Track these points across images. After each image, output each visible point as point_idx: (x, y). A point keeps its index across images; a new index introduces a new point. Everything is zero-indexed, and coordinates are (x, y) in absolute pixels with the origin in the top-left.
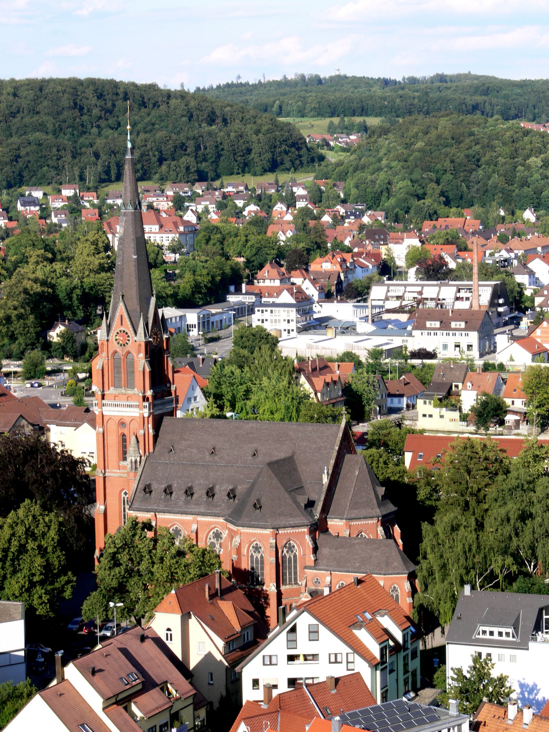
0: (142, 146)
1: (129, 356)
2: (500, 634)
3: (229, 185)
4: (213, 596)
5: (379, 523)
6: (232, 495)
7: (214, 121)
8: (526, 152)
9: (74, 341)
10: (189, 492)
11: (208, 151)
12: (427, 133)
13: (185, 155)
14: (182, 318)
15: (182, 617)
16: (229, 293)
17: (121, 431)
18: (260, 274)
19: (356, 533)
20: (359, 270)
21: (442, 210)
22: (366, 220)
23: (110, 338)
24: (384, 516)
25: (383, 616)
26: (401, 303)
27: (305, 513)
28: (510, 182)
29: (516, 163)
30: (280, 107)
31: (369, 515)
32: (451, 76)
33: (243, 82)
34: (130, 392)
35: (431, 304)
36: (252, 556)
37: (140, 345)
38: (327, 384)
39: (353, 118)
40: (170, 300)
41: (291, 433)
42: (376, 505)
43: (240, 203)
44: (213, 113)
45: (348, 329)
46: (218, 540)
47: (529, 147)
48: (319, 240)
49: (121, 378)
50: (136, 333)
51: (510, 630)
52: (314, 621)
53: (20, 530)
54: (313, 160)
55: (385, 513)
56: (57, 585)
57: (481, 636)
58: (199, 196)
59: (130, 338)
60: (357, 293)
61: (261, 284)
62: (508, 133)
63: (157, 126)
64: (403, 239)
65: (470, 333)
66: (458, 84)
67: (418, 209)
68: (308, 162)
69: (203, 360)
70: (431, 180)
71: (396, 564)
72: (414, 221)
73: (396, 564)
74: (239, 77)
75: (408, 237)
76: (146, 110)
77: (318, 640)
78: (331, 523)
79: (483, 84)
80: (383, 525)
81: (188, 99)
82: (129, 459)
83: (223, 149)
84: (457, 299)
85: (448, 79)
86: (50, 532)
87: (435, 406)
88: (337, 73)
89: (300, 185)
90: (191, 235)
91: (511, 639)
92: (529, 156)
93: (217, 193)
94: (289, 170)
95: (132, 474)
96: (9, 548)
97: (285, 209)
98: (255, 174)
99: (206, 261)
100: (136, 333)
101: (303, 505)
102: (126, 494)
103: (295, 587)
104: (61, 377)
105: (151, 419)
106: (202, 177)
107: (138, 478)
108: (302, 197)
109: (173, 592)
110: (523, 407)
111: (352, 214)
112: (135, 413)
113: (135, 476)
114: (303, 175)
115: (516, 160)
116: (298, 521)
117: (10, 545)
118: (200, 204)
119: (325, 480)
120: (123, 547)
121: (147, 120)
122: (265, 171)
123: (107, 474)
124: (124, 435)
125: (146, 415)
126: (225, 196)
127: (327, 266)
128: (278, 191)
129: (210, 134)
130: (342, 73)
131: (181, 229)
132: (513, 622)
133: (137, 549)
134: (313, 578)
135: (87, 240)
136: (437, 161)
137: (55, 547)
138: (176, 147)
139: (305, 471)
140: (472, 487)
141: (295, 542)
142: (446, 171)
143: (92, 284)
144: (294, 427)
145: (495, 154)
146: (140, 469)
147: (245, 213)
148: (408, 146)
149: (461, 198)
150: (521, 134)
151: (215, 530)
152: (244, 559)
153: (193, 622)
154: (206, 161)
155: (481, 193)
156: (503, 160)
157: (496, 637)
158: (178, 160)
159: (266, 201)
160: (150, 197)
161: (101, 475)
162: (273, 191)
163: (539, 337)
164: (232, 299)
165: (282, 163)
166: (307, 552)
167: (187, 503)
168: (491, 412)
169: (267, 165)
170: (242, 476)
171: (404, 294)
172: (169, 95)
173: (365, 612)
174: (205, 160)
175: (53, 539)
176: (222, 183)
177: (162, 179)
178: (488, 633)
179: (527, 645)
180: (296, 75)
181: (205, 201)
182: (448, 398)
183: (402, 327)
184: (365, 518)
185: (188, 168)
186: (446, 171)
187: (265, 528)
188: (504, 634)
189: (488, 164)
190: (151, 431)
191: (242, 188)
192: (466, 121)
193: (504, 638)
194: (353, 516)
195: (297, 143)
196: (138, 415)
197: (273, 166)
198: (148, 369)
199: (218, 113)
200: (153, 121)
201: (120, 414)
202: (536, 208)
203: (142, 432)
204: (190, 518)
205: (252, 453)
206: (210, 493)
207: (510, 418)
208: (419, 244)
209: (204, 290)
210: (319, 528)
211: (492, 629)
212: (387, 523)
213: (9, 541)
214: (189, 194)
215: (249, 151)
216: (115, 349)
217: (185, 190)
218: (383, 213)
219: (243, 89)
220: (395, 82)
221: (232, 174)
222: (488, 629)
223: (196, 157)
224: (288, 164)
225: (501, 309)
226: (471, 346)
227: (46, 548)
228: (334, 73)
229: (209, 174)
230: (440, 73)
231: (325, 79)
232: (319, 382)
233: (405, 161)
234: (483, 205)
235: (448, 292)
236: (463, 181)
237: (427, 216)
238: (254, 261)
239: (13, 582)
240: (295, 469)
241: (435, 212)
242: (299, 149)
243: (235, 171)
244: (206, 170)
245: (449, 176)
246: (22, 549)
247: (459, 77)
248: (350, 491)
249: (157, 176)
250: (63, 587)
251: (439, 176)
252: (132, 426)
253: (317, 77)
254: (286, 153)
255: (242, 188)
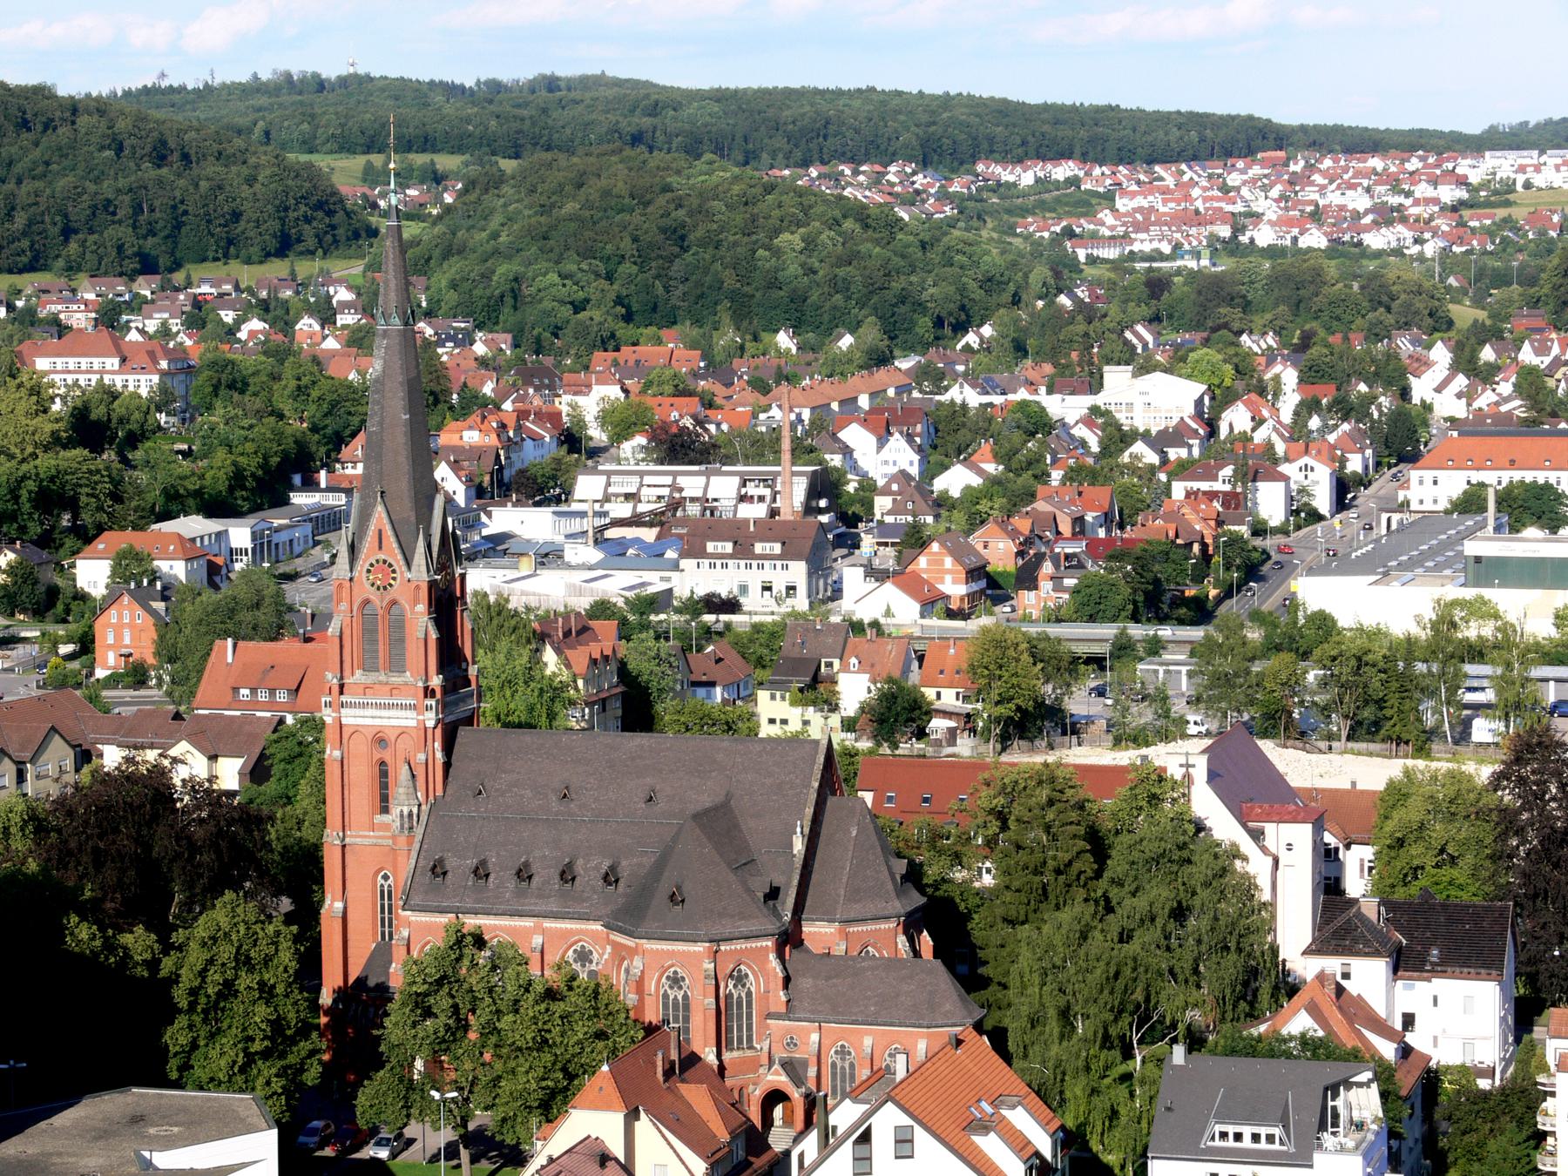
0: (30, 205)
1: (395, 610)
2: (1256, 1138)
3: (203, 281)
4: (669, 1073)
5: (900, 928)
6: (610, 878)
7: (163, 158)
8: (774, 222)
9: (36, 582)
10: (524, 874)
11: (158, 215)
12: (580, 186)
13: (114, 222)
14: (221, 536)
15: (626, 1116)
16: (293, 488)
17: (377, 756)
18: (345, 452)
19: (858, 949)
20: (529, 444)
21: (623, 331)
22: (480, 349)
23: (356, 574)
24: (909, 915)
25: (1013, 1107)
26: (635, 507)
27: (765, 911)
28: (743, 279)
29: (755, 242)
30: (267, 134)
31: (881, 914)
32: (569, 80)
33: (176, 85)
34: (396, 679)
35: (693, 510)
36: (666, 996)
37: (418, 587)
38: (594, 662)
39: (411, 156)
40: (191, 502)
41: (720, 757)
42: (893, 894)
43: (228, 317)
44: (164, 143)
45: (549, 557)
46: (583, 966)
47: (776, 213)
48: (437, 389)
49: (377, 651)
50: (409, 565)
51: (1277, 1131)
52: (906, 1120)
53: (226, 952)
54: (357, 235)
55: (909, 909)
56: (292, 1059)
57: (1218, 1143)
58: (146, 302)
59: (397, 575)
60: (544, 488)
61: (349, 471)
62: (736, 188)
63: (54, 167)
64: (589, 386)
65: (790, 563)
66: (596, 94)
67: (580, 328)
68: (348, 239)
69: (313, 616)
70: (598, 275)
71: (948, 1007)
72: (572, 352)
73: (948, 1007)
74: (163, 75)
75: (599, 382)
76: (31, 136)
77: (912, 1157)
78: (807, 929)
79: (647, 96)
80: (906, 932)
81: (112, 115)
82: (395, 811)
83: (186, 213)
84: (743, 498)
85: (562, 84)
86: (281, 954)
87: (793, 703)
88: (351, 70)
89: (339, 281)
90: (182, 377)
91: (1276, 1146)
92: (777, 232)
93: (182, 297)
94: (313, 253)
95: (402, 840)
96: (200, 987)
97: (317, 327)
98: (248, 262)
99: (251, 426)
100: (409, 565)
101: (760, 895)
102: (386, 877)
103: (749, 1053)
104: (20, 651)
105: (439, 731)
106: (148, 266)
107: (417, 846)
108: (345, 305)
109: (605, 1068)
110: (959, 703)
111: (450, 338)
112: (409, 719)
113: (410, 843)
114: (340, 264)
115: (754, 237)
116: (754, 927)
117: (204, 981)
118: (151, 317)
119: (799, 845)
120: (440, 983)
121: (36, 153)
122: (267, 255)
123: (347, 840)
124: (383, 763)
125: (431, 724)
126: (198, 303)
127: (472, 437)
128: (297, 293)
129: (160, 182)
130: (361, 71)
131: (164, 364)
132: (1279, 1114)
133: (466, 986)
134: (783, 1037)
135: (20, 386)
136: (605, 237)
137: (290, 985)
138: (94, 208)
139: (753, 828)
140: (1055, 858)
141: (750, 967)
142: (623, 257)
143: (53, 472)
144: (726, 744)
145: (715, 226)
146: (419, 831)
147: (242, 335)
148: (545, 209)
149: (654, 309)
150: (758, 190)
151: (578, 947)
152: (649, 1001)
153: (644, 1125)
154: (155, 235)
155: (692, 299)
156: (731, 238)
157: (1247, 1143)
158: (101, 233)
159: (280, 312)
160: (53, 303)
161: (337, 842)
162: (289, 293)
163: (926, 571)
164: (300, 499)
165: (299, 241)
166: (772, 986)
167: (520, 894)
168: (898, 713)
169: (273, 244)
170: (629, 841)
171: (639, 490)
172: (74, 108)
173: (979, 1101)
174: (152, 233)
175: (286, 970)
176: (188, 277)
177: (70, 269)
178: (1231, 1136)
179: (1311, 1158)
180: (275, 71)
181: (160, 311)
182: (815, 688)
183: (654, 556)
184: (876, 919)
185: (120, 248)
186: (623, 257)
187: (694, 940)
188: (1263, 1138)
189: (703, 244)
190: (439, 755)
191: (228, 287)
192: (652, 164)
193: (1263, 1145)
194: (852, 916)
195: (327, 202)
196: (413, 723)
197: (284, 247)
198: (433, 635)
199: (172, 144)
200: (46, 158)
201: (377, 722)
202: (797, 328)
203: (421, 757)
204: (528, 923)
205: (644, 795)
206: (567, 875)
207: (938, 725)
208: (622, 396)
209: (250, 483)
210: (789, 939)
211: (1238, 1129)
212: (911, 926)
213: (203, 974)
214: (127, 297)
215: (236, 216)
216: (365, 596)
217: (120, 289)
218: (509, 337)
219: (176, 98)
220: (462, 88)
221: (204, 260)
222: (1231, 1129)
223: (134, 227)
224: (311, 242)
225: (824, 519)
226: (794, 588)
227: (274, 986)
228: (345, 70)
229: (161, 261)
230: (548, 73)
231: (328, 80)
232: (579, 658)
233: (544, 239)
234: (698, 322)
235: (724, 487)
236: (658, 277)
237: (599, 343)
238: (326, 426)
239: (213, 1054)
240: (736, 826)
241: (613, 336)
242: (330, 213)
243: (211, 255)
244: (153, 253)
245: (627, 268)
246: (228, 989)
247: (586, 82)
248: (843, 868)
249: (61, 263)
250: (302, 1063)
251: (611, 267)
252: (401, 745)
253: (316, 76)
254: (308, 220)
255: (228, 287)
